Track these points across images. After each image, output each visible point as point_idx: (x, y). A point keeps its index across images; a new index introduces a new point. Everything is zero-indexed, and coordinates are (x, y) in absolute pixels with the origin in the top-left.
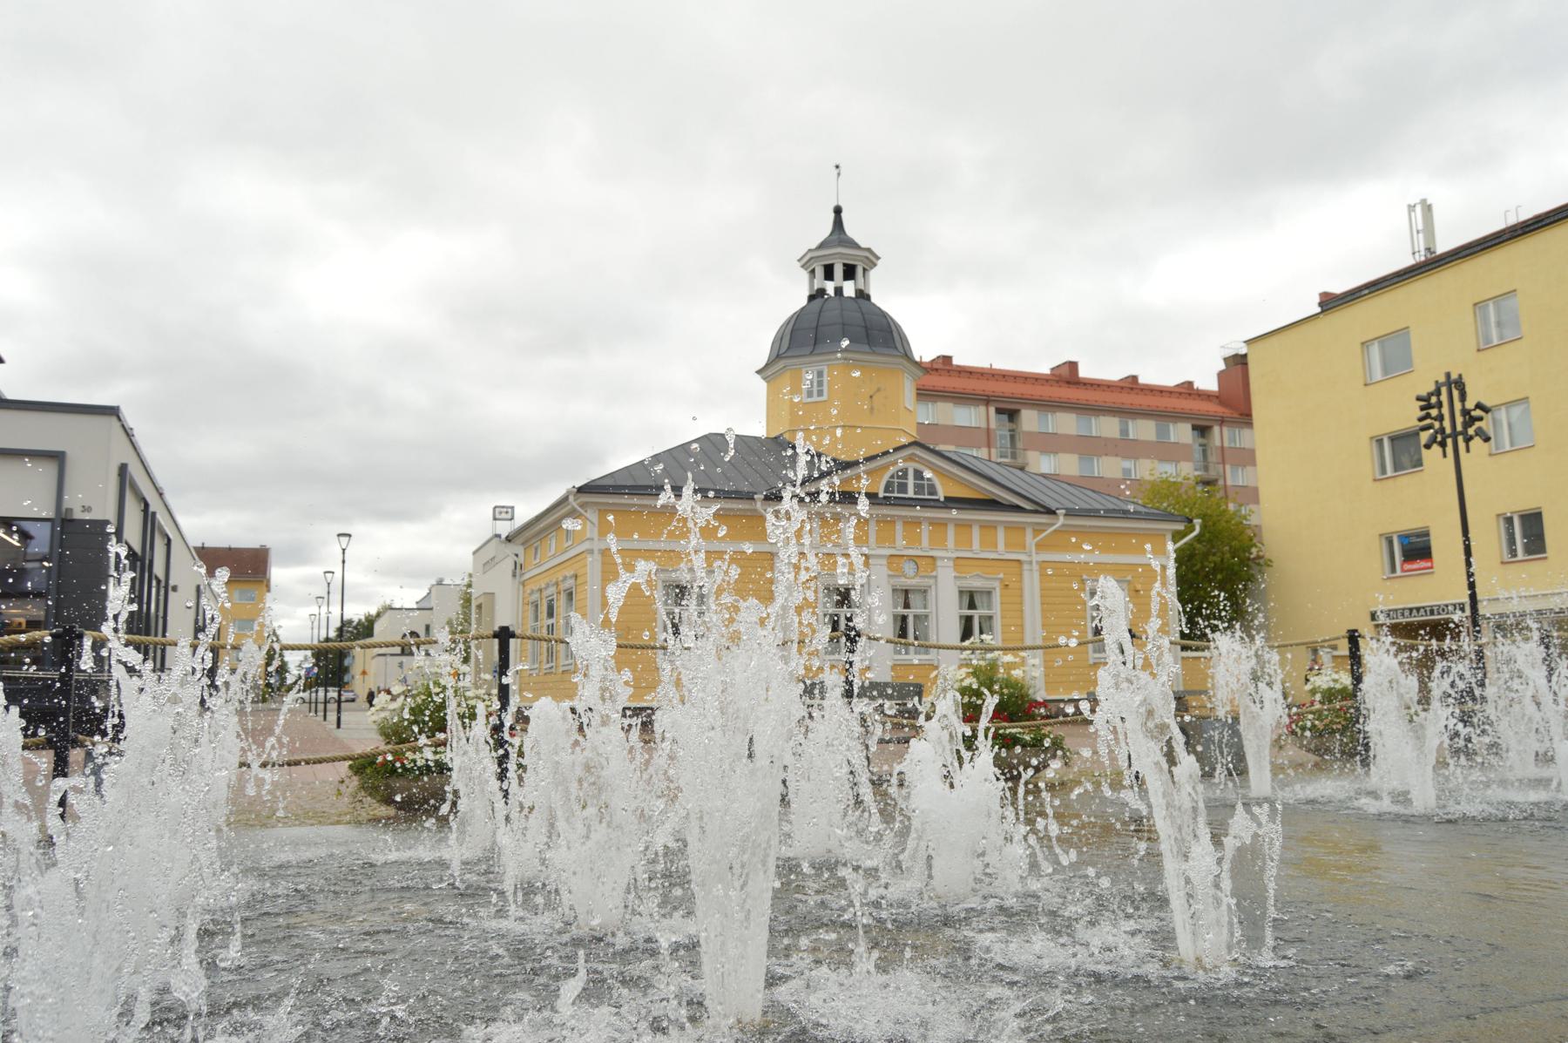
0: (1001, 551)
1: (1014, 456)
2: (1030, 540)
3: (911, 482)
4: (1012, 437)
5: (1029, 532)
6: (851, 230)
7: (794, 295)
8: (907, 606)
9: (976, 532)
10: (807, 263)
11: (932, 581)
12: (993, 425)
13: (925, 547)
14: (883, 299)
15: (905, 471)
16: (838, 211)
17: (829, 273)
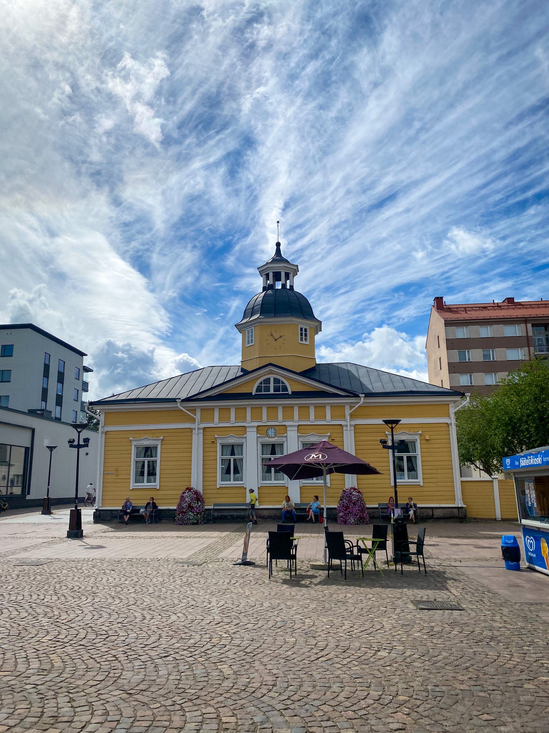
0: (233, 421)
3: (272, 385)
5: (347, 408)
9: (312, 411)
11: (284, 439)
12: (530, 334)
15: (267, 381)
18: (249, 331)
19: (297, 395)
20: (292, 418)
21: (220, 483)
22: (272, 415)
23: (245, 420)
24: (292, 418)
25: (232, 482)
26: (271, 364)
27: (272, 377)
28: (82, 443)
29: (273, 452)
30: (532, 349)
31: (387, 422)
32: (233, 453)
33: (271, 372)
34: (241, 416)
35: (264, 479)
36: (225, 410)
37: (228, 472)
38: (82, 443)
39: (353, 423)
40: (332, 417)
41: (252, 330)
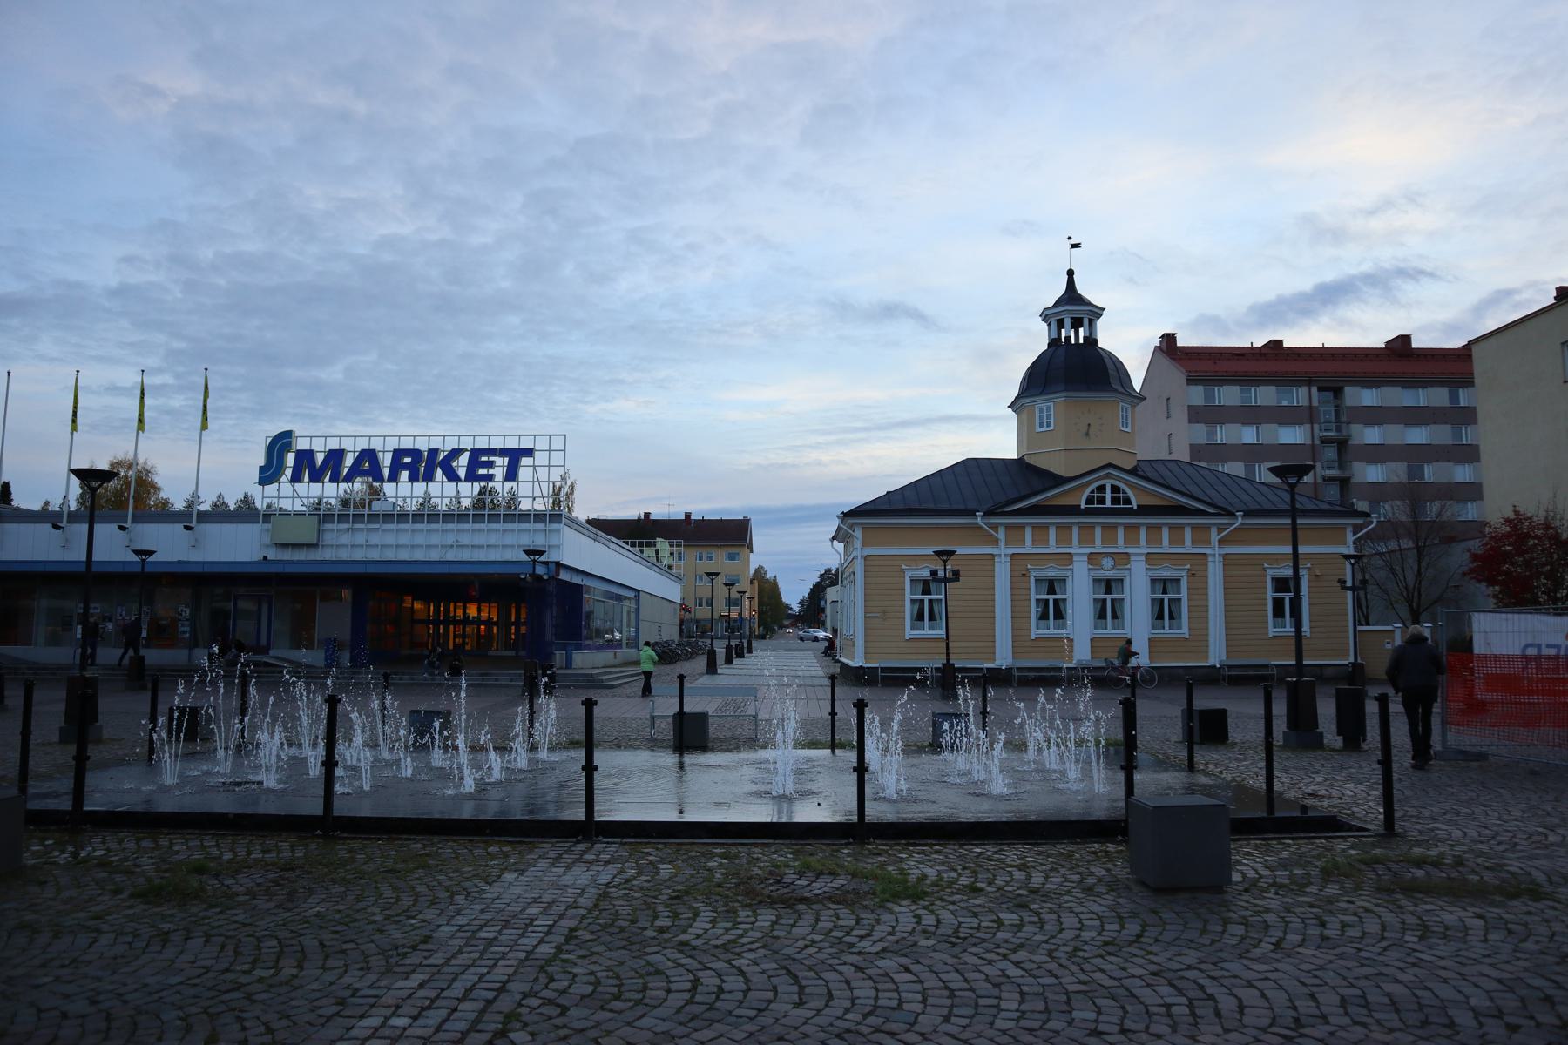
0: (1188, 546)
1: (1338, 430)
2: (1215, 536)
4: (1337, 413)
5: (1214, 531)
6: (1081, 289)
7: (1037, 340)
8: (1165, 592)
10: (1046, 316)
12: (1315, 403)
13: (1120, 545)
14: (1105, 341)
15: (1102, 488)
16: (1070, 273)
17: (1061, 324)
18: (1041, 410)
19: (1144, 510)
20: (1137, 542)
21: (1034, 634)
22: (1109, 538)
23: (1208, 542)
24: (1137, 542)
25: (1052, 631)
26: (1110, 465)
27: (1108, 483)
28: (949, 575)
29: (1108, 591)
30: (1316, 426)
31: (938, 554)
32: (1051, 591)
33: (1108, 476)
34: (1064, 539)
35: (1154, 627)
36: (1040, 529)
37: (920, 617)
38: (949, 575)
39: (866, 553)
40: (1193, 542)
41: (1048, 408)
